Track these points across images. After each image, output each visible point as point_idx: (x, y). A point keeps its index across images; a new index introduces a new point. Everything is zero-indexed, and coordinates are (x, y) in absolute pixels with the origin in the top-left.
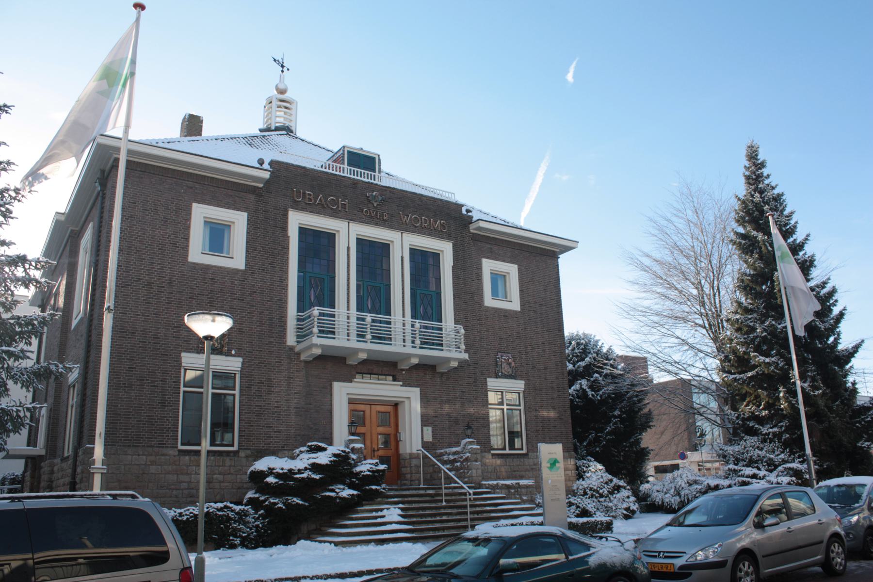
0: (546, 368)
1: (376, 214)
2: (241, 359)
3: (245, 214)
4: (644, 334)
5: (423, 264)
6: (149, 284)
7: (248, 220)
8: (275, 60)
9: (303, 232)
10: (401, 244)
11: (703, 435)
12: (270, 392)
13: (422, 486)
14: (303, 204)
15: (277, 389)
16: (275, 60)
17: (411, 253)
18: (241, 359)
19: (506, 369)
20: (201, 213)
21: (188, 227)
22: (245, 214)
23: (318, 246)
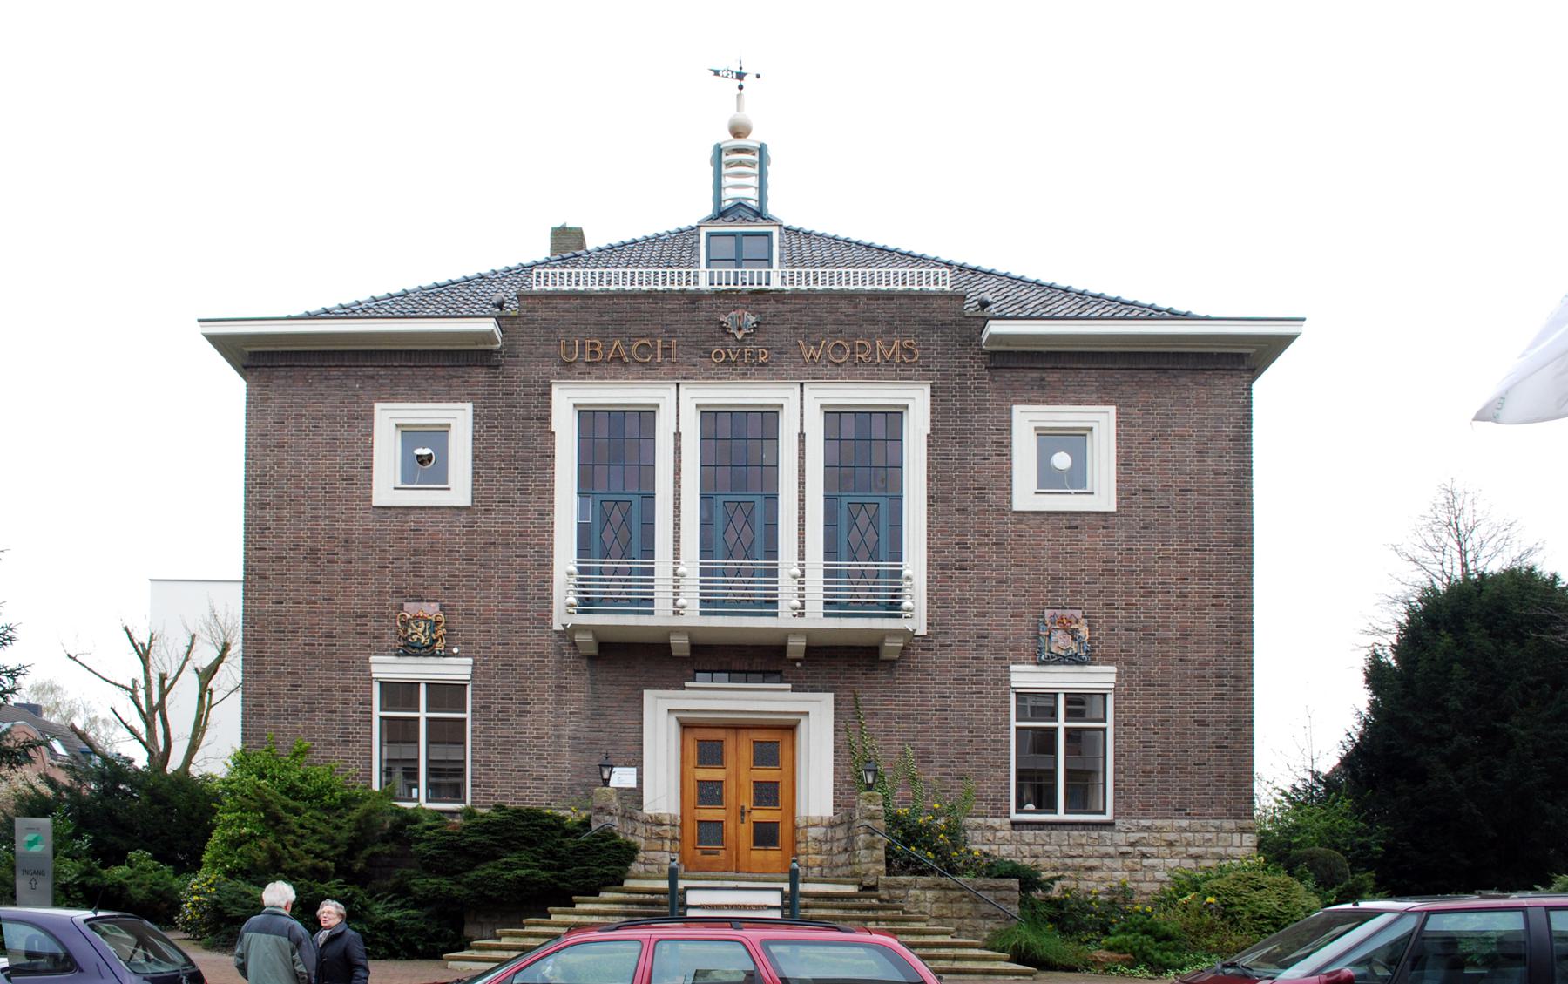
0: (1185, 636)
1: (742, 355)
2: (470, 660)
3: (469, 406)
4: (212, 670)
5: (861, 450)
6: (313, 552)
7: (475, 415)
8: (716, 73)
9: (587, 415)
10: (802, 411)
11: (1067, 891)
12: (523, 714)
13: (1061, 816)
14: (582, 366)
15: (537, 708)
16: (716, 73)
17: (707, 439)
18: (470, 660)
19: (1060, 642)
20: (389, 419)
21: (369, 448)
22: (469, 406)
23: (618, 444)
